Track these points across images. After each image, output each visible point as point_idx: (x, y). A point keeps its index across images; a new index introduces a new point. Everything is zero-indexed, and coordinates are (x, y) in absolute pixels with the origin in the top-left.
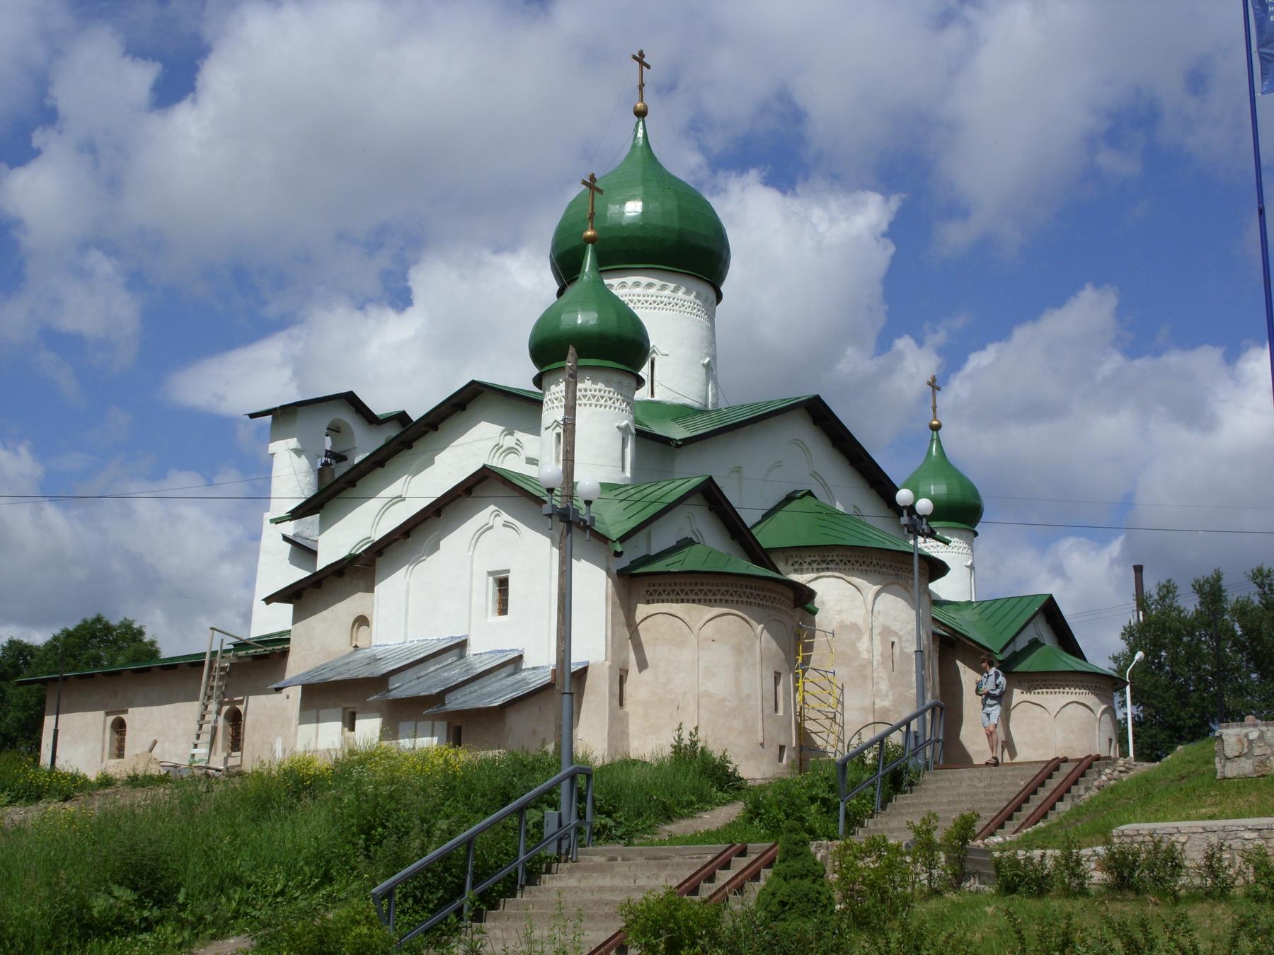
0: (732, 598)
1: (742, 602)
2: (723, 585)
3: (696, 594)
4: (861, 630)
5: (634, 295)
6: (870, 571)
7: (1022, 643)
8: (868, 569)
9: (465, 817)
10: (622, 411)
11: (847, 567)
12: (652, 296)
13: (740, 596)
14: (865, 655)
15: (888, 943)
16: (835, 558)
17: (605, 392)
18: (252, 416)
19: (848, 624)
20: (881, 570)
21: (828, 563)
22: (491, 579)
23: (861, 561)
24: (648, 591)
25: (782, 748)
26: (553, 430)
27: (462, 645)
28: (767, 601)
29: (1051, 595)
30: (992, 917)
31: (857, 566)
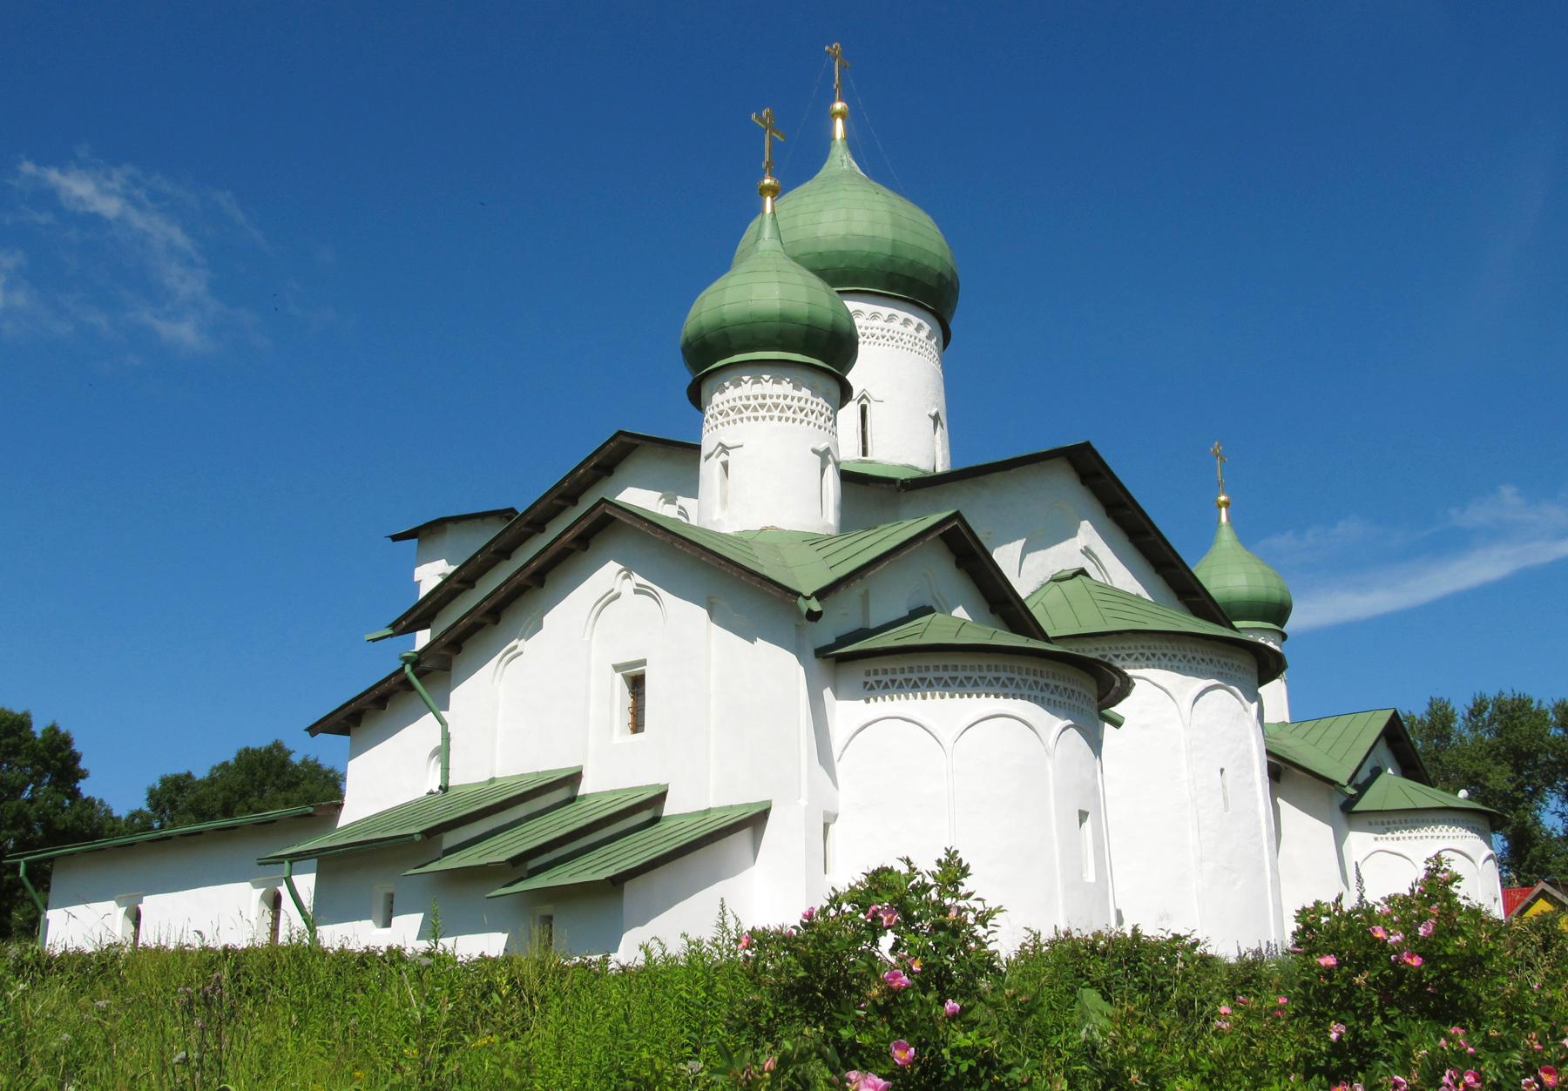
10: (820, 427)
17: (793, 399)
18: (395, 538)
20: (1199, 667)
22: (619, 676)
24: (866, 683)
26: (717, 457)
27: (574, 779)
30: (1196, 1071)
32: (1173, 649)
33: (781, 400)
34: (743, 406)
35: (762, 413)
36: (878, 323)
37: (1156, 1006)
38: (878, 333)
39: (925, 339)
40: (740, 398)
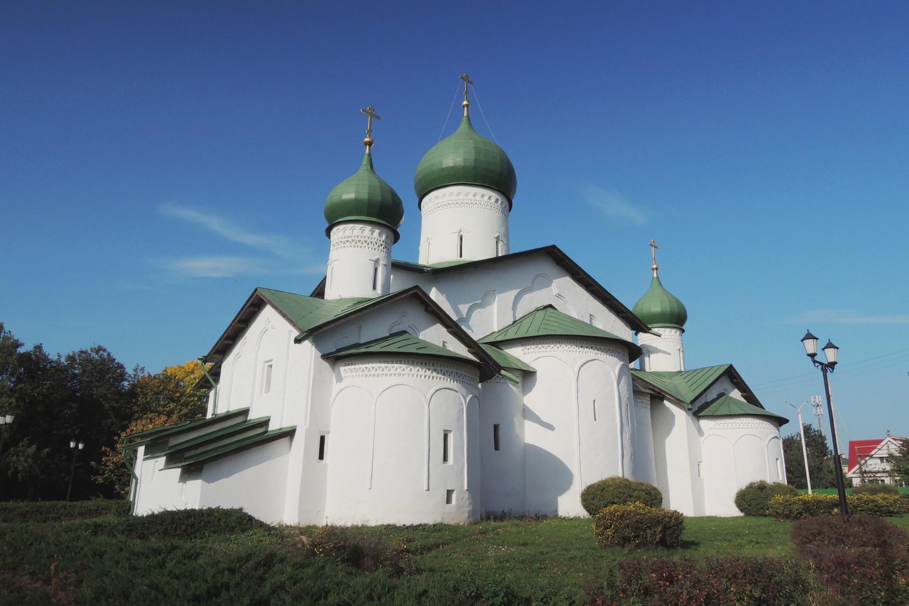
5: (450, 200)
7: (711, 395)
9: (203, 550)
12: (456, 200)
15: (640, 587)
25: (449, 493)
36: (454, 197)
37: (451, 572)
38: (469, 202)
39: (494, 203)
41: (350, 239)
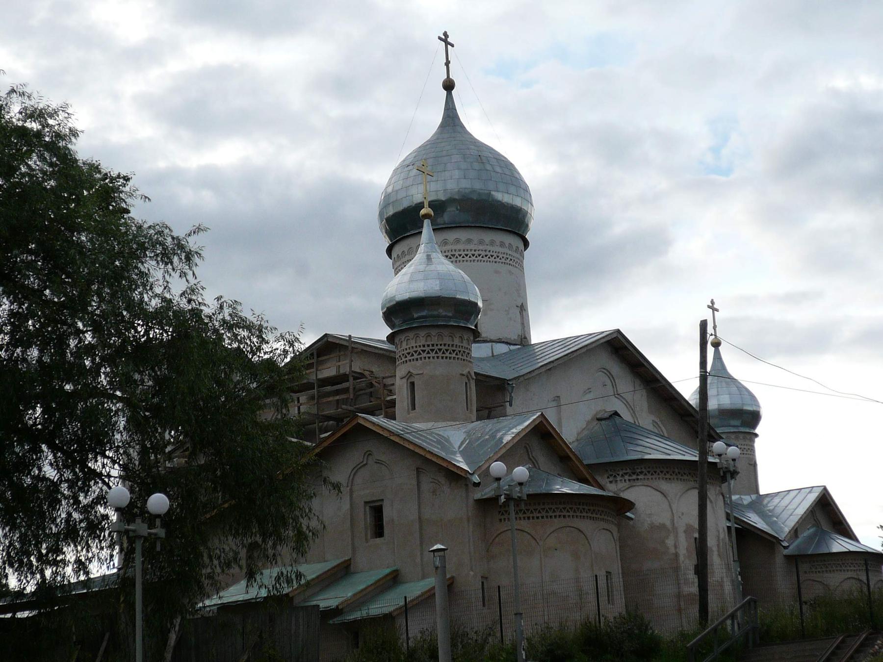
0: (568, 514)
1: (577, 516)
2: (539, 504)
3: (539, 512)
4: (669, 530)
6: (674, 479)
8: (672, 477)
11: (654, 477)
12: (471, 250)
13: (575, 512)
14: (672, 550)
16: (643, 470)
19: (658, 525)
21: (638, 475)
23: (665, 470)
24: (500, 512)
28: (596, 514)
29: (825, 489)
31: (662, 475)
32: (667, 468)
33: (442, 347)
34: (422, 350)
35: (432, 354)
40: (420, 346)
41: (436, 348)
